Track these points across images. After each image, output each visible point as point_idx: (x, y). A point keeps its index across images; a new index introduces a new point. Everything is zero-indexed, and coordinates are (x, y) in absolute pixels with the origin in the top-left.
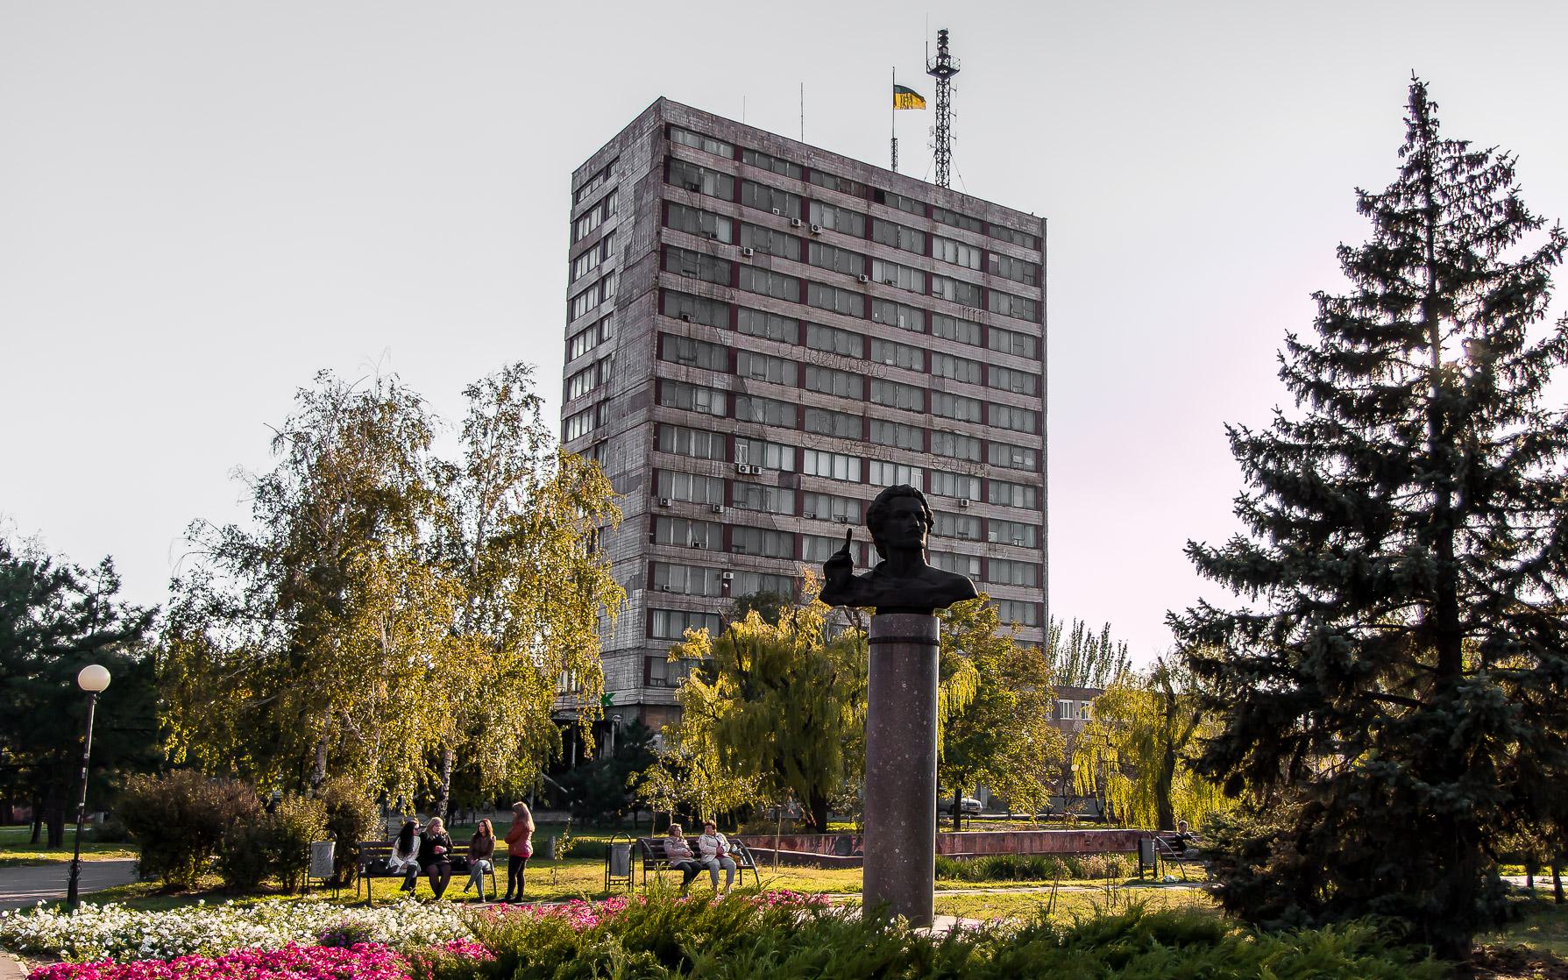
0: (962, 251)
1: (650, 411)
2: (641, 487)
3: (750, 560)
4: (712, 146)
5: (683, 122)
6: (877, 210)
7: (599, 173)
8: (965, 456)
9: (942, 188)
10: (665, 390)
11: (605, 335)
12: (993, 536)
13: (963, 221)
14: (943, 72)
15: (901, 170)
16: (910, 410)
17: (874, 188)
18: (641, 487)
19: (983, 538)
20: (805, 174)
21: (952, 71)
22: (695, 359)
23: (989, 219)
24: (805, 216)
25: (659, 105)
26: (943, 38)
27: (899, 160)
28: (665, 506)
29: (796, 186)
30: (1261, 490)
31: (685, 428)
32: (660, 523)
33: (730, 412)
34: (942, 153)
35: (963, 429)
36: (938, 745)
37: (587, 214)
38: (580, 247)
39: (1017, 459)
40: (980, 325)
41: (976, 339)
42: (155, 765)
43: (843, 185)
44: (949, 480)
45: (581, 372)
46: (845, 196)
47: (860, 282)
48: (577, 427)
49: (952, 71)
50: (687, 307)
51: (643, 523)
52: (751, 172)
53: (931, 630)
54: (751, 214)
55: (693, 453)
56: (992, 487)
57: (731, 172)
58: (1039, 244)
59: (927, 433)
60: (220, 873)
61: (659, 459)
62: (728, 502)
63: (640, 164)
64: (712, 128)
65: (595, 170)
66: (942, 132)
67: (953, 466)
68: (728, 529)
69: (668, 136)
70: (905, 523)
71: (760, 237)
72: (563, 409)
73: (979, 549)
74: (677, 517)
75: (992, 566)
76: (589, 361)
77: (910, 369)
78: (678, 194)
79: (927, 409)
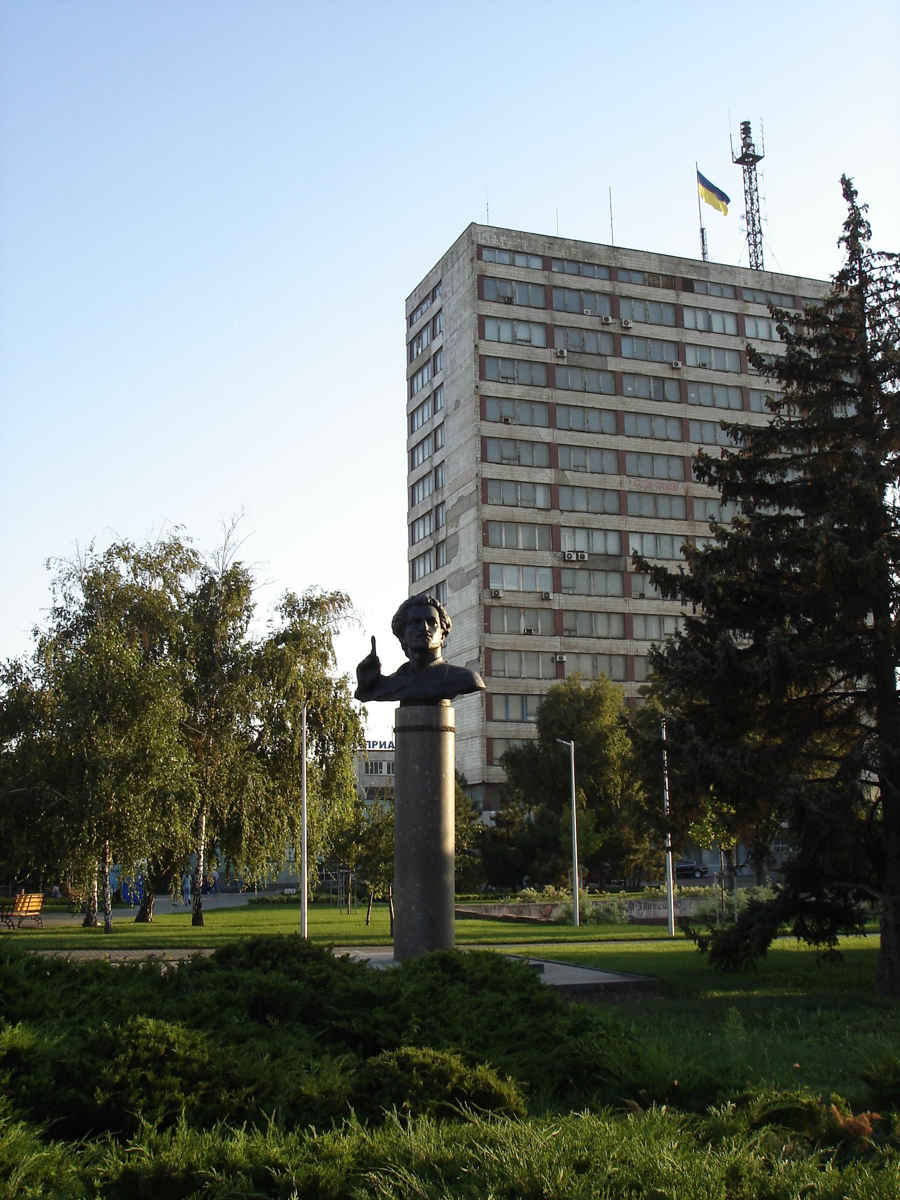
1: (478, 510)
3: (582, 642)
4: (520, 260)
5: (494, 243)
6: (686, 298)
10: (492, 489)
14: (748, 159)
15: (711, 258)
17: (681, 278)
18: (474, 581)
20: (613, 273)
22: (518, 458)
23: (801, 293)
24: (615, 313)
26: (746, 129)
29: (607, 286)
30: (690, 604)
32: (494, 613)
33: (554, 504)
34: (754, 235)
36: (450, 844)
38: (416, 365)
42: (640, 789)
43: (652, 279)
46: (653, 289)
47: (675, 369)
49: (759, 158)
52: (559, 280)
54: (562, 318)
57: (541, 281)
61: (490, 555)
63: (460, 286)
64: (519, 245)
66: (751, 217)
68: (557, 615)
71: (574, 338)
72: (409, 514)
76: (427, 469)
78: (493, 309)
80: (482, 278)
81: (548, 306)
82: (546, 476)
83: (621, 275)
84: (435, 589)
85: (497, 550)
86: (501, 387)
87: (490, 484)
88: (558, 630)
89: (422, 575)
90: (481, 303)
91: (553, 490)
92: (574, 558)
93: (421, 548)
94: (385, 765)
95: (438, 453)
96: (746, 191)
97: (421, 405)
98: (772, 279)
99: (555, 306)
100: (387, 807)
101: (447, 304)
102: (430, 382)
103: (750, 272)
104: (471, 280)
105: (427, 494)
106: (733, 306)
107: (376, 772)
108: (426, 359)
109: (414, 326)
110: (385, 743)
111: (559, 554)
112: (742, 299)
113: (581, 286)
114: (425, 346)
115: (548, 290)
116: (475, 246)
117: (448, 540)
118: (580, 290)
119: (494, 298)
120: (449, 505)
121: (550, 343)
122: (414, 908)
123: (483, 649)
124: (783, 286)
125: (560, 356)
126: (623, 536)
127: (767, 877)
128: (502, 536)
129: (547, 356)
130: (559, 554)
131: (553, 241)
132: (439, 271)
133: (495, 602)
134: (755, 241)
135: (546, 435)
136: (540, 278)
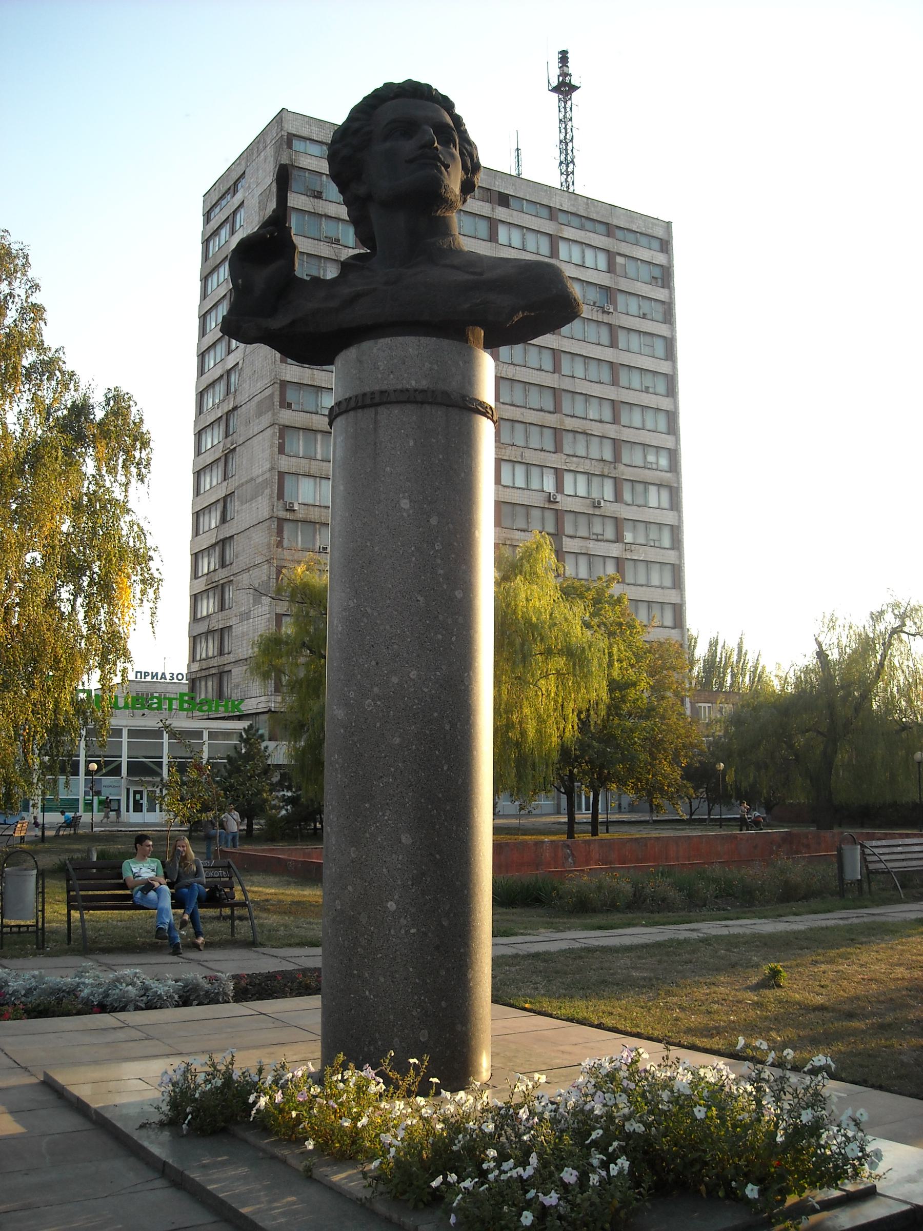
0: (589, 253)
1: (274, 415)
2: (267, 492)
5: (304, 132)
6: (501, 213)
7: (227, 192)
8: (598, 457)
9: (567, 191)
12: (628, 537)
13: (589, 225)
16: (541, 410)
19: (619, 539)
21: (574, 88)
23: (615, 222)
25: (282, 116)
26: (564, 58)
27: (523, 162)
28: (292, 510)
32: (287, 527)
34: (567, 164)
35: (596, 428)
37: (216, 232)
38: (209, 304)
39: (651, 458)
40: (608, 251)
41: (605, 339)
44: (582, 480)
45: (212, 385)
49: (574, 88)
51: (269, 528)
53: (469, 375)
56: (627, 487)
58: (665, 246)
59: (558, 433)
65: (223, 190)
67: (586, 466)
69: (290, 146)
70: (408, 147)
72: (196, 422)
73: (615, 550)
74: (304, 521)
75: (629, 566)
77: (540, 370)
79: (557, 410)
84: (222, 503)
85: (294, 459)
89: (208, 487)
93: (208, 458)
95: (232, 355)
96: (561, 120)
98: (587, 204)
103: (566, 194)
106: (548, 227)
109: (212, 223)
110: (157, 673)
112: (556, 220)
114: (223, 242)
122: (392, 906)
124: (598, 213)
126: (554, 240)
128: (299, 444)
132: (243, 163)
133: (288, 516)
134: (567, 171)
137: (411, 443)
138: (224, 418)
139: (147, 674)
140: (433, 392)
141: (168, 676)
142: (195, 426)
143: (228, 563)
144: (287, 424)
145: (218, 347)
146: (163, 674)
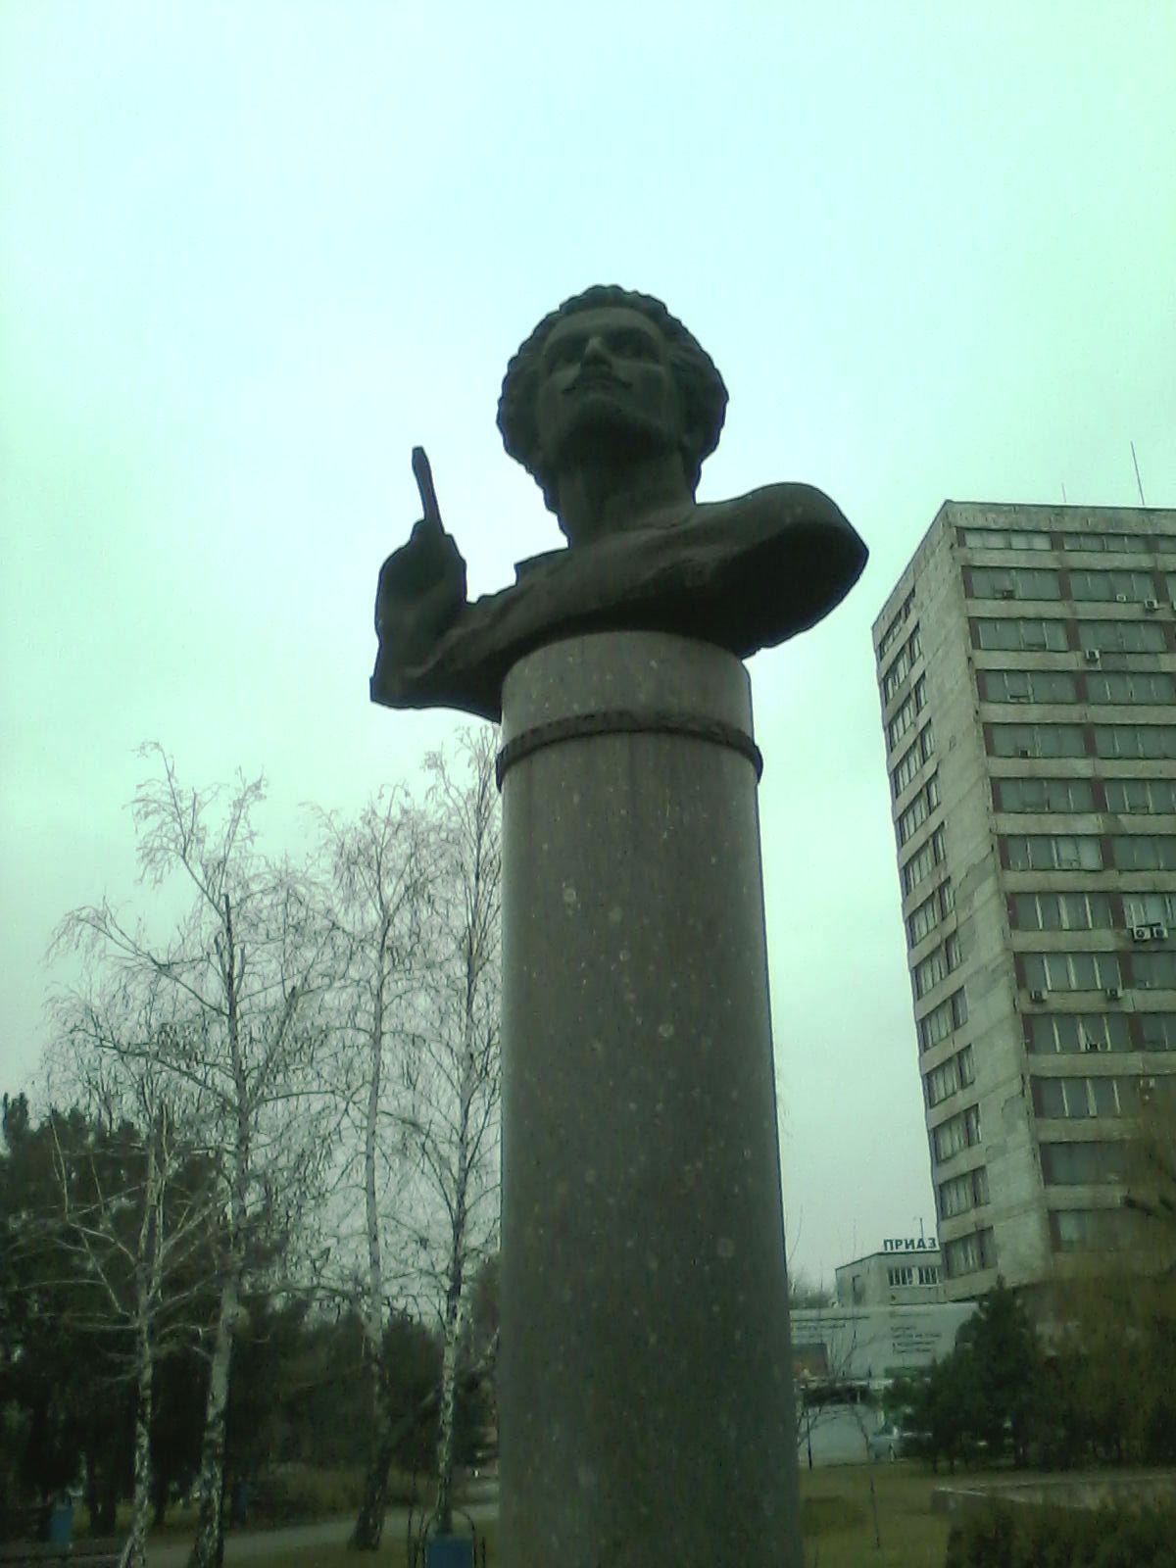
4: (1018, 542)
5: (980, 522)
11: (934, 802)
29: (1145, 561)
31: (1049, 896)
33: (1108, 862)
48: (935, 1029)
50: (1023, 739)
52: (1077, 560)
54: (1086, 610)
55: (1066, 925)
60: (878, 1414)
62: (1129, 981)
71: (1106, 635)
80: (968, 570)
81: (1065, 595)
82: (1091, 824)
83: (1164, 545)
86: (1010, 708)
87: (1011, 843)
88: (1138, 1043)
90: (969, 602)
91: (1105, 842)
92: (1147, 935)
93: (925, 948)
94: (915, 1273)
97: (906, 757)
99: (1075, 595)
100: (1157, 1510)
101: (925, 617)
102: (914, 724)
104: (953, 575)
105: (925, 874)
107: (904, 1283)
108: (906, 694)
109: (885, 658)
110: (912, 1241)
111: (1125, 932)
113: (1107, 565)
115: (1063, 575)
116: (954, 530)
117: (960, 932)
118: (1106, 571)
119: (988, 592)
120: (955, 883)
121: (1074, 645)
123: (1028, 1078)
125: (1092, 660)
127: (148, 1374)
129: (1073, 661)
130: (1125, 932)
131: (1060, 510)
135: (1083, 767)
136: (1049, 561)
137: (576, 799)
138: (937, 894)
139: (898, 1242)
140: (605, 715)
141: (928, 1243)
142: (903, 909)
143: (969, 1081)
144: (1017, 889)
145: (917, 807)
146: (921, 1240)
